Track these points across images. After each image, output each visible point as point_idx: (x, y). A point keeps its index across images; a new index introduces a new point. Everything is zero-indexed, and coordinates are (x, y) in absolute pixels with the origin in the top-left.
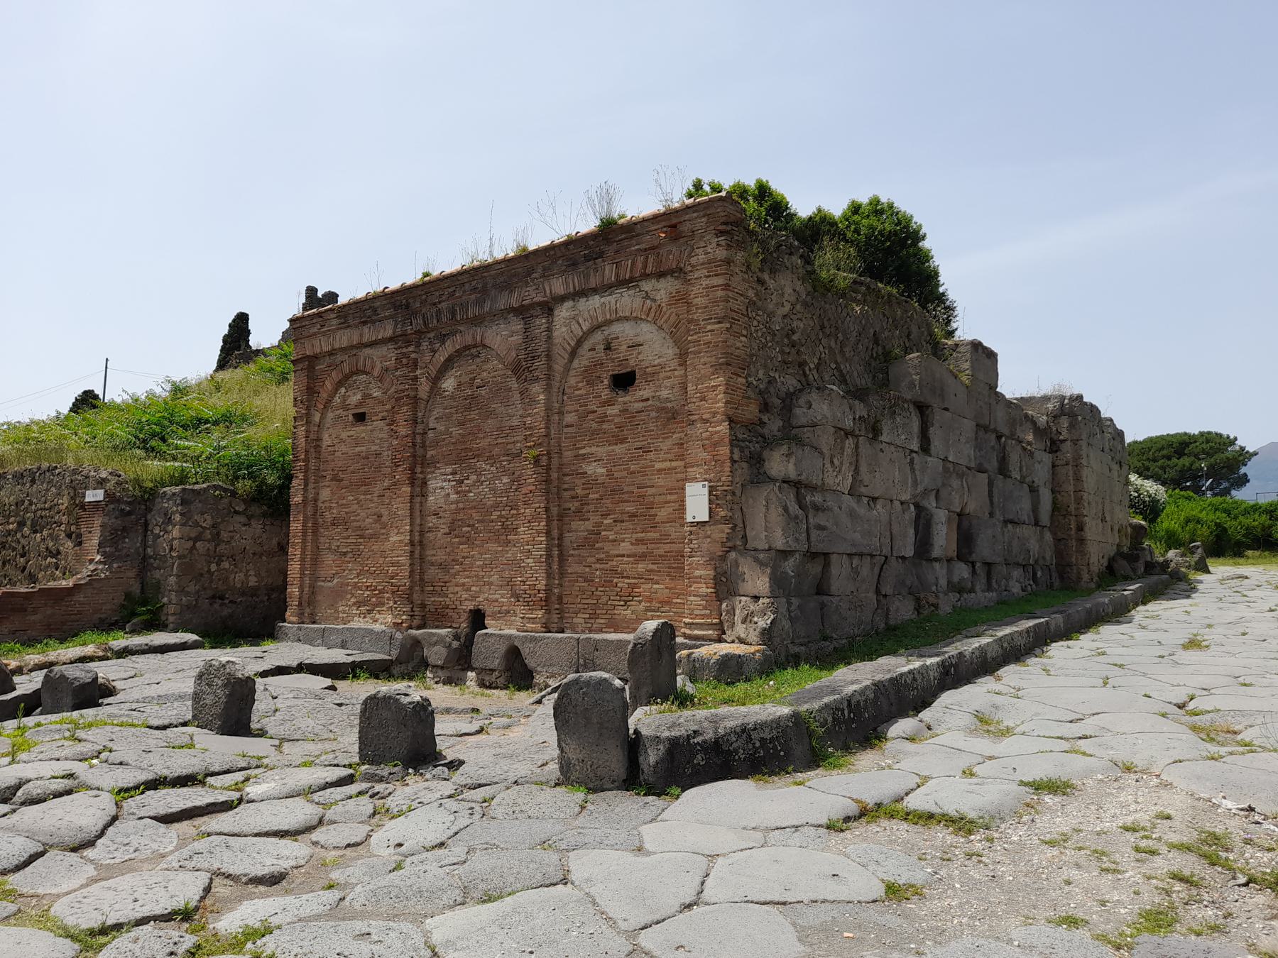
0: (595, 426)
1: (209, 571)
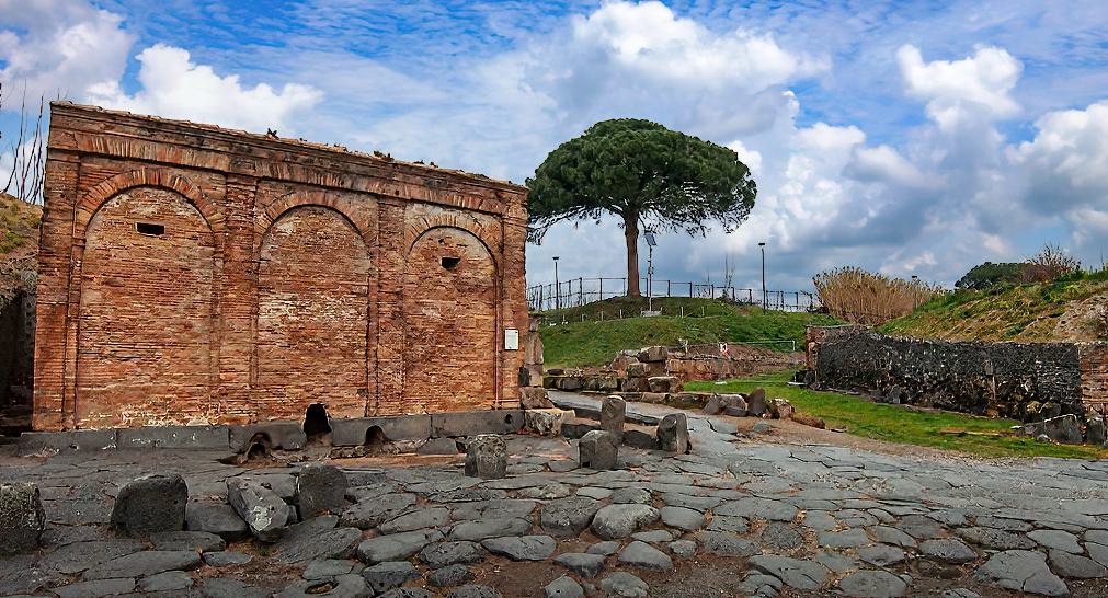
0: (431, 286)
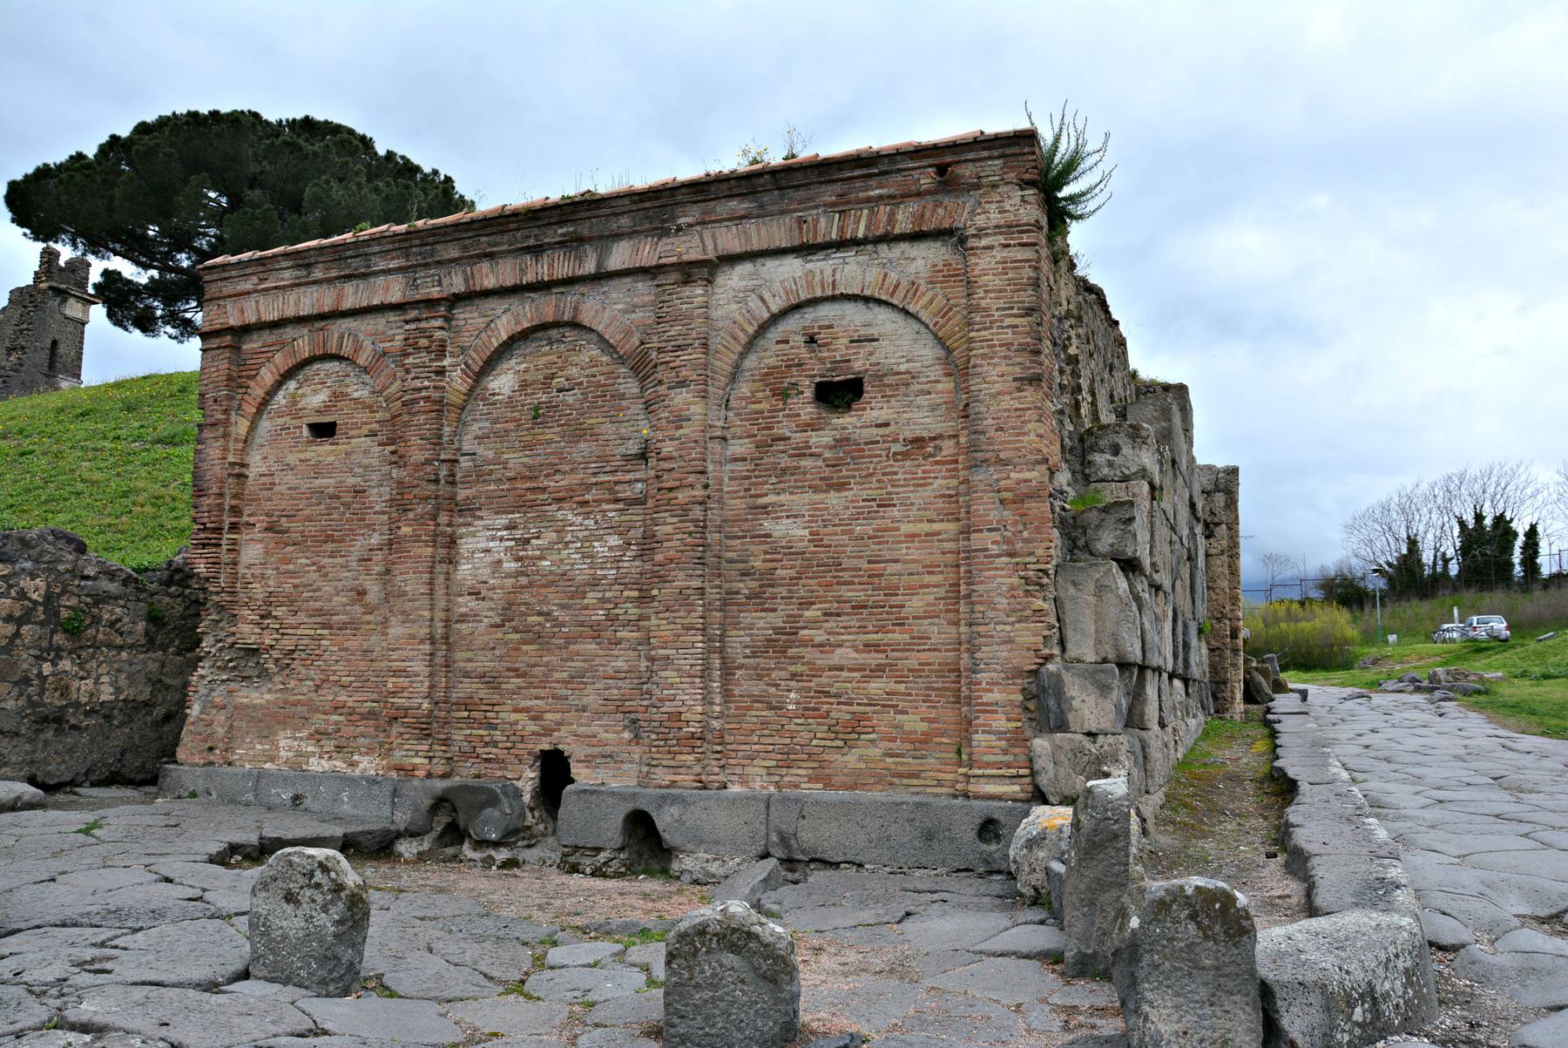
0: (785, 461)
1: (40, 674)
